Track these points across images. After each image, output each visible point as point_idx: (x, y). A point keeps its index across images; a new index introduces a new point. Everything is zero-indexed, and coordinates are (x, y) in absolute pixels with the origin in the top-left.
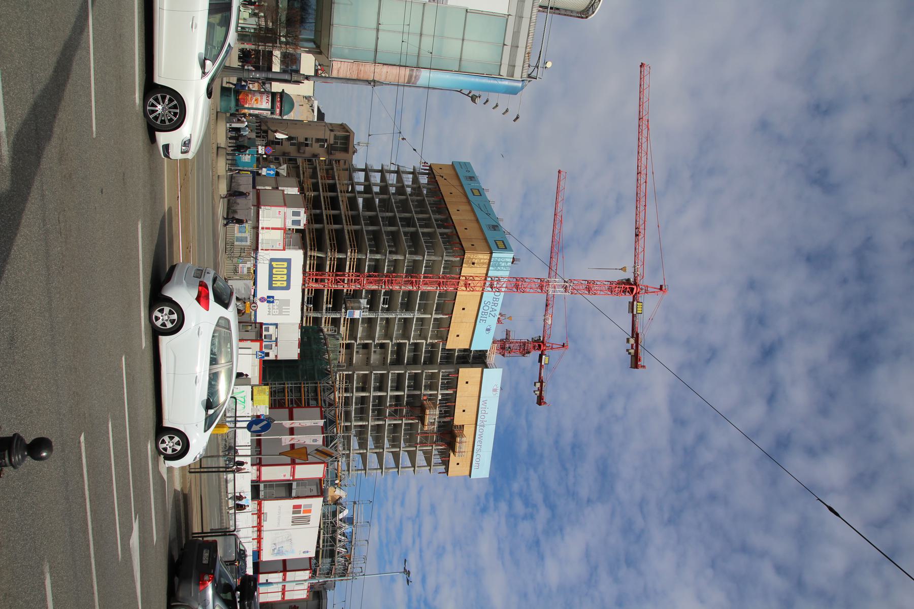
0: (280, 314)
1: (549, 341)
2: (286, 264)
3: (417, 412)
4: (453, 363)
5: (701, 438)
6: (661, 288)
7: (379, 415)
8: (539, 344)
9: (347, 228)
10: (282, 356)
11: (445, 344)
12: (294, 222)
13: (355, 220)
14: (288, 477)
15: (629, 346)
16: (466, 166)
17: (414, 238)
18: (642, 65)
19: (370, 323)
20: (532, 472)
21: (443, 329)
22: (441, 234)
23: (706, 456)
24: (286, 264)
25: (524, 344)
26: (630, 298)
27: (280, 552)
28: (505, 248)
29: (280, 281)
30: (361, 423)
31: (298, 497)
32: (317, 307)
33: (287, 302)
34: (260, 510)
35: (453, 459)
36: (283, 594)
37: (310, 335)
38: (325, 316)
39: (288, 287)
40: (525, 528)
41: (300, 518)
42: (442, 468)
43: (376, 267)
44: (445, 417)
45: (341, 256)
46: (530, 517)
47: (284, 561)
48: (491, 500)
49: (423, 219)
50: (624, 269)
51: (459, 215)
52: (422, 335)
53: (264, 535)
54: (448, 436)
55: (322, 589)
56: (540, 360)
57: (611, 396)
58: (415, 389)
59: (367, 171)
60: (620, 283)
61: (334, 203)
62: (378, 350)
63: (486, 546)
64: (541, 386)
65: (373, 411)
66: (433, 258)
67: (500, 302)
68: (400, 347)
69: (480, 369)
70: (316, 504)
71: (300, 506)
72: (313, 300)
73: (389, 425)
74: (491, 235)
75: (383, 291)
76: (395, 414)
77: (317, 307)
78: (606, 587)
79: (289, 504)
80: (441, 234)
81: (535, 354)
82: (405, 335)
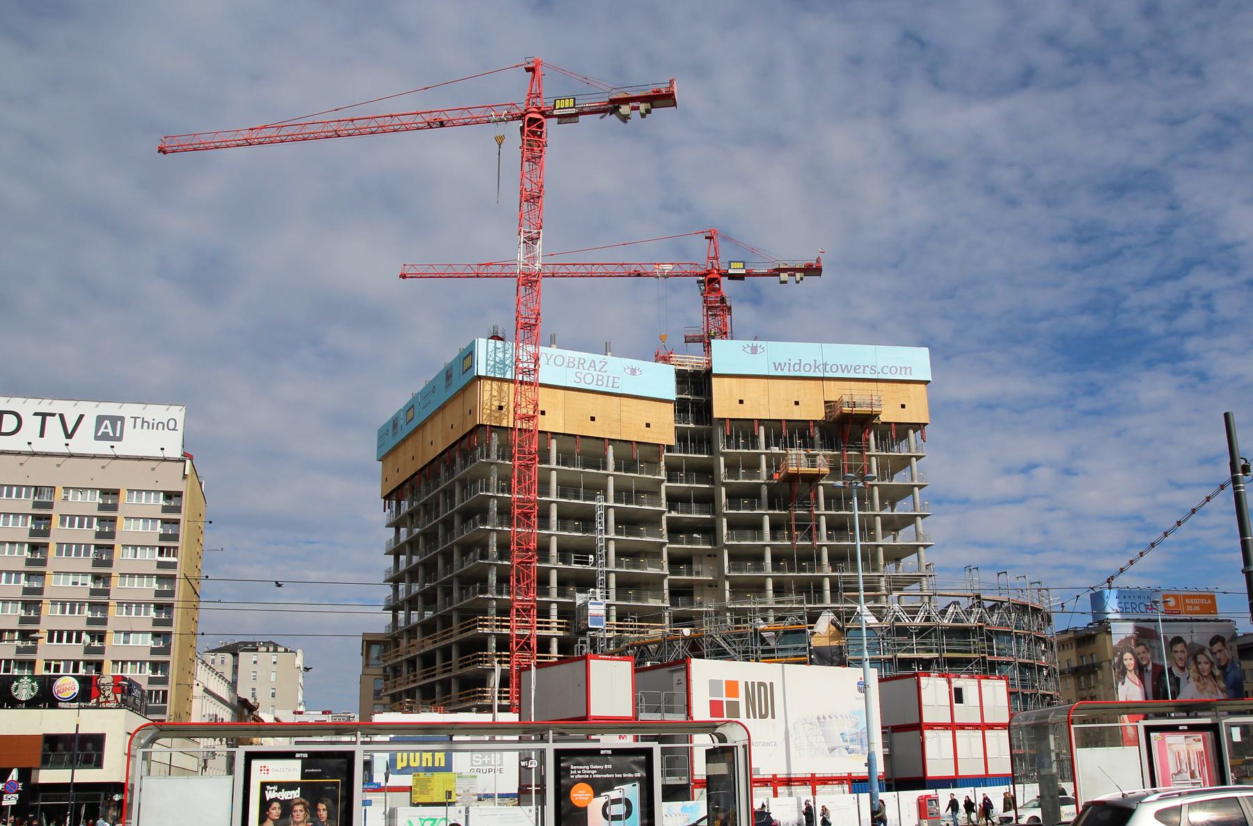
1: (704, 264)
3: (800, 487)
4: (711, 431)
5: (1052, 40)
7: (809, 558)
8: (710, 281)
15: (635, 115)
16: (382, 434)
18: (162, 150)
21: (636, 455)
23: (1082, 29)
26: (550, 124)
28: (469, 355)
30: (827, 593)
35: (889, 414)
36: (991, 727)
40: (1227, 306)
44: (812, 438)
50: (500, 140)
51: (437, 441)
53: (799, 771)
54: (845, 428)
55: (1235, 645)
56: (739, 277)
57: (991, 190)
58: (759, 497)
64: (785, 270)
65: (802, 569)
68: (675, 529)
69: (714, 380)
73: (829, 538)
75: (560, 565)
76: (808, 527)
81: (726, 285)
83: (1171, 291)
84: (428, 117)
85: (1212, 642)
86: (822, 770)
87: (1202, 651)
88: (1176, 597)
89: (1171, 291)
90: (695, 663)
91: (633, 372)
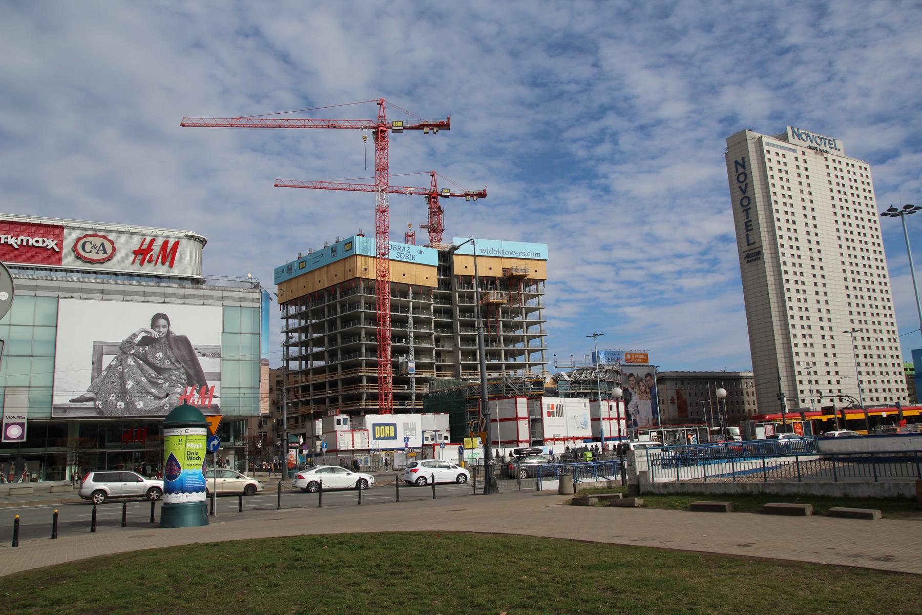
0: (414, 429)
2: (377, 428)
6: (380, 104)
8: (432, 197)
9: (339, 376)
10: (447, 426)
11: (435, 288)
12: (345, 423)
13: (333, 369)
14: (527, 421)
17: (346, 320)
19: (418, 352)
20: (565, 135)
21: (421, 291)
22: (341, 297)
24: (377, 428)
25: (432, 212)
27: (585, 424)
28: (350, 243)
29: (389, 431)
31: (542, 414)
32: (408, 397)
33: (406, 425)
34: (551, 440)
35: (532, 275)
36: (612, 419)
37: (430, 405)
38: (414, 390)
39: (394, 425)
40: (627, 142)
41: (558, 412)
42: (540, 285)
43: (372, 350)
45: (365, 380)
46: (614, 137)
47: (592, 420)
48: (596, 182)
49: (329, 311)
50: (365, 138)
51: (324, 281)
52: (427, 308)
53: (570, 435)
54: (512, 281)
56: (447, 196)
57: (477, 40)
59: (287, 359)
60: (376, 139)
61: (320, 387)
62: (441, 344)
63: (646, 187)
66: (362, 304)
67: (397, 244)
68: (438, 325)
70: (546, 401)
71: (549, 413)
72: (402, 404)
73: (504, 331)
74: (340, 255)
76: (494, 326)
77: (408, 397)
78: (690, 45)
79: (547, 420)
80: (341, 297)
82: (427, 322)
83: (593, 128)
84: (327, 122)
85: (646, 376)
86: (577, 435)
87: (641, 380)
88: (631, 354)
89: (593, 128)
90: (543, 398)
91: (421, 252)
